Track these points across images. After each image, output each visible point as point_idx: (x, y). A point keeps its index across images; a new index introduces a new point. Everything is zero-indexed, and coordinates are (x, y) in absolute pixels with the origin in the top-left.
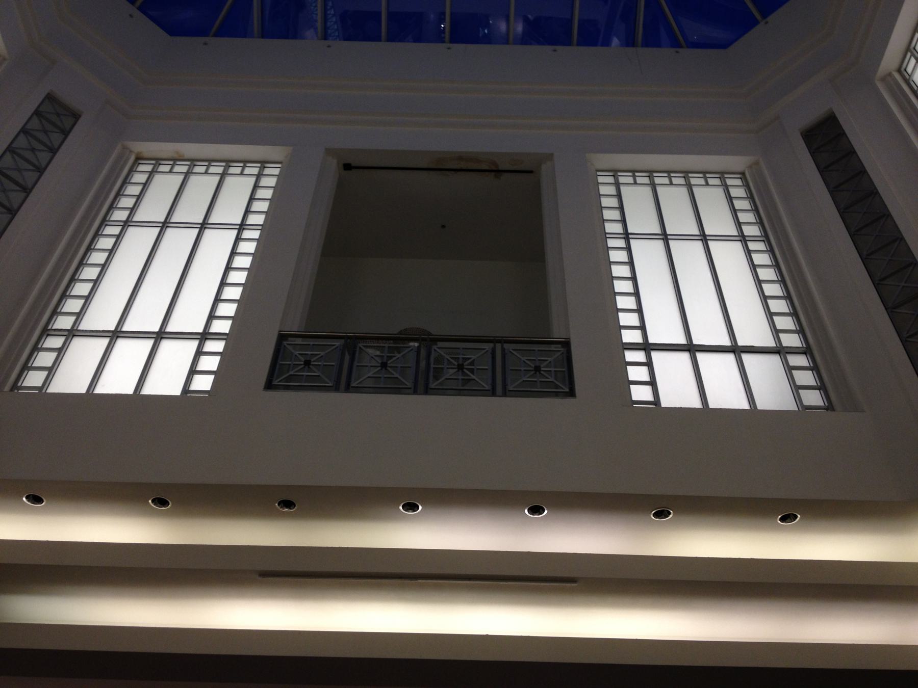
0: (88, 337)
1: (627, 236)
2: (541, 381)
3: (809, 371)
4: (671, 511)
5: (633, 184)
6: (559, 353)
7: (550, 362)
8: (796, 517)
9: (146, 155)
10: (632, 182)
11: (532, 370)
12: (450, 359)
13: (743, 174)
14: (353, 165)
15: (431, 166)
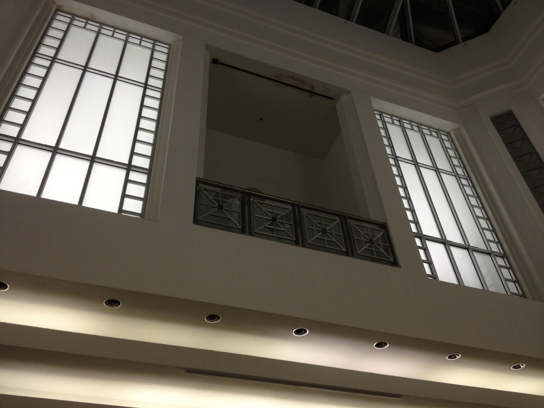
0: (99, 163)
1: (146, 86)
2: (276, 229)
3: (506, 269)
4: (8, 286)
5: (110, 36)
6: (289, 210)
7: (282, 216)
8: (306, 331)
9: (65, 9)
10: (138, 43)
11: (216, 208)
12: (316, 223)
13: (449, 133)
14: (220, 61)
15: (272, 78)
